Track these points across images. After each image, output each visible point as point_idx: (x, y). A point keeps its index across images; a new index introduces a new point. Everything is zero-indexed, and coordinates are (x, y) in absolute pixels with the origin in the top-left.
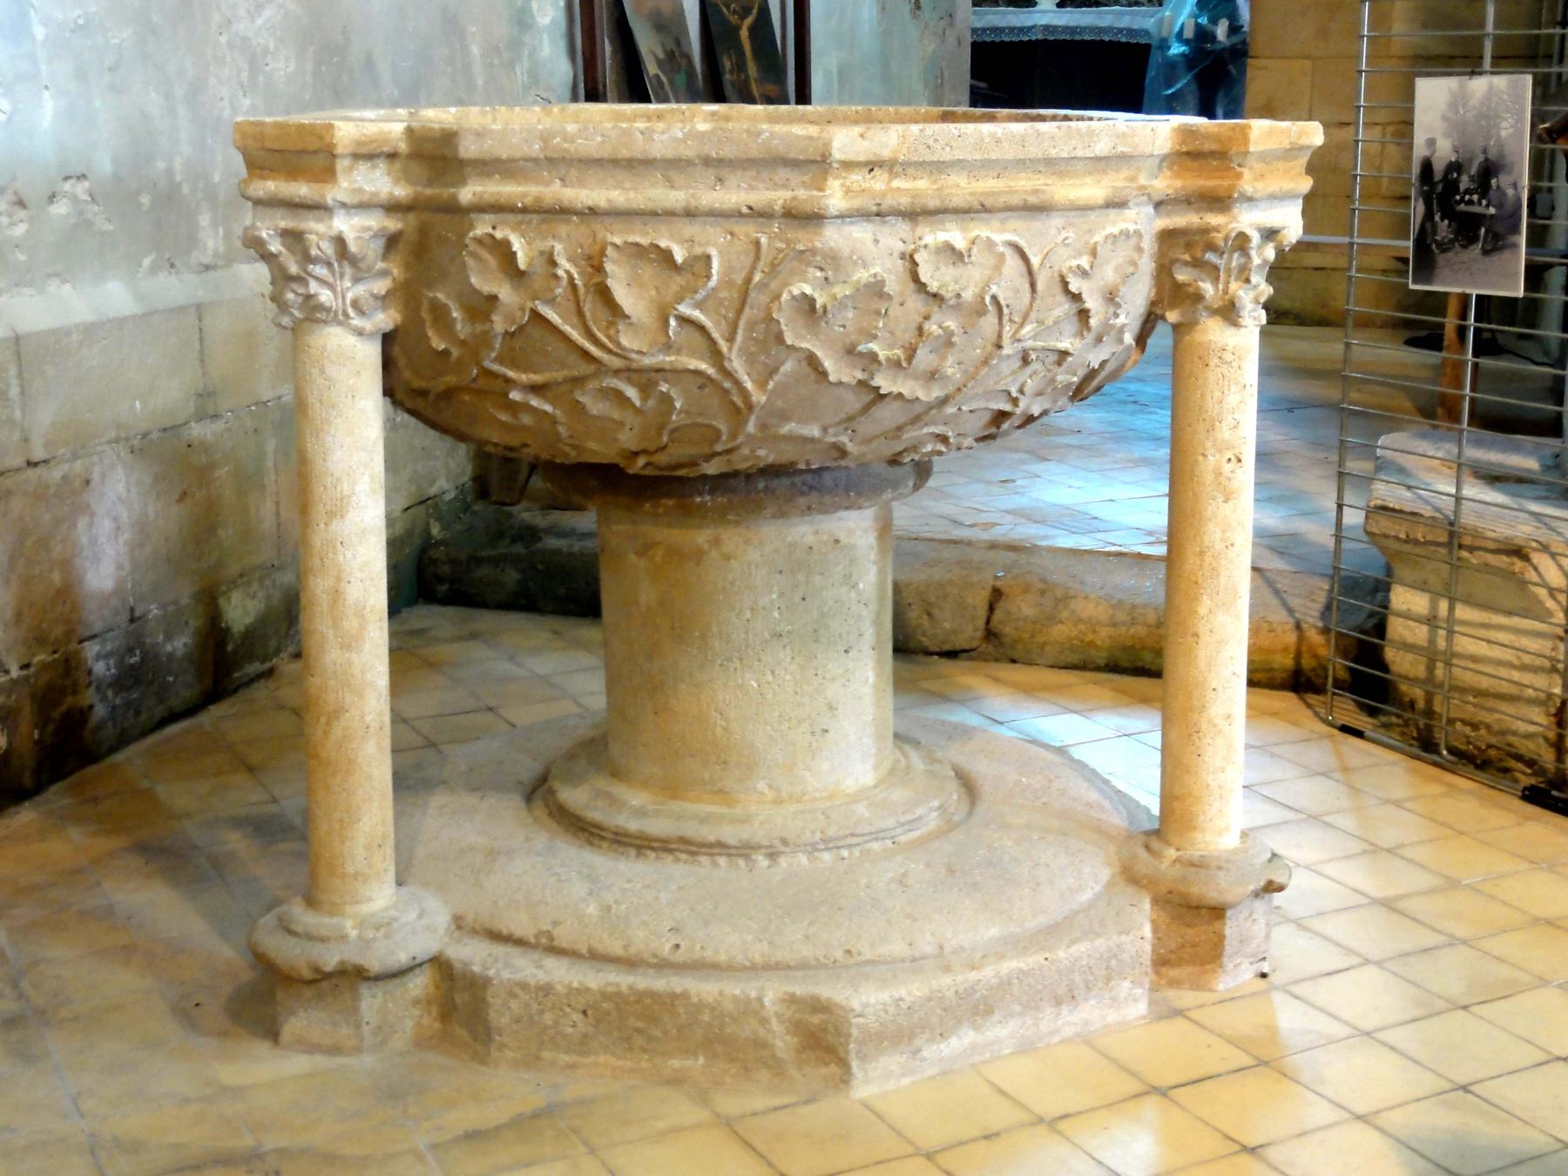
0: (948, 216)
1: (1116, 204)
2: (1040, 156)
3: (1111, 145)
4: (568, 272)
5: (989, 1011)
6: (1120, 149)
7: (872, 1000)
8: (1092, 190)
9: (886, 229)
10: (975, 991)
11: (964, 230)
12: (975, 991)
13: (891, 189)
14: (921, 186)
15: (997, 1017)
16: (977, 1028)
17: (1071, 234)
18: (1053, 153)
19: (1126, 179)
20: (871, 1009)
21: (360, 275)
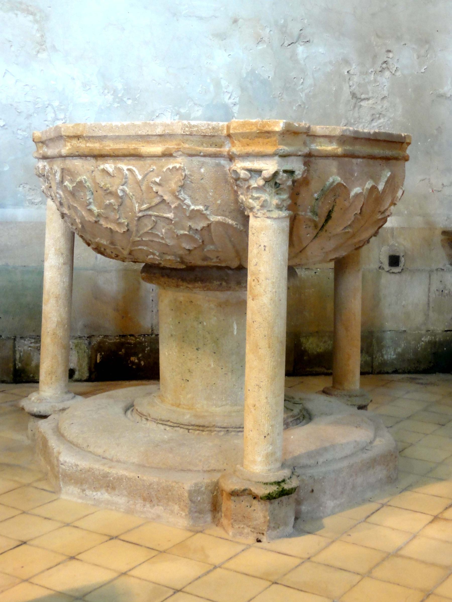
0: (109, 158)
1: (167, 155)
2: (134, 134)
3: (163, 129)
4: (128, 170)
5: (114, 488)
6: (167, 131)
7: (67, 461)
8: (158, 149)
9: (87, 162)
10: (107, 477)
11: (114, 163)
12: (107, 477)
13: (87, 147)
14: (96, 146)
15: (117, 492)
16: (7, 265)
17: (154, 167)
18: (140, 133)
19: (176, 145)
20: (67, 464)
21: (279, 192)
